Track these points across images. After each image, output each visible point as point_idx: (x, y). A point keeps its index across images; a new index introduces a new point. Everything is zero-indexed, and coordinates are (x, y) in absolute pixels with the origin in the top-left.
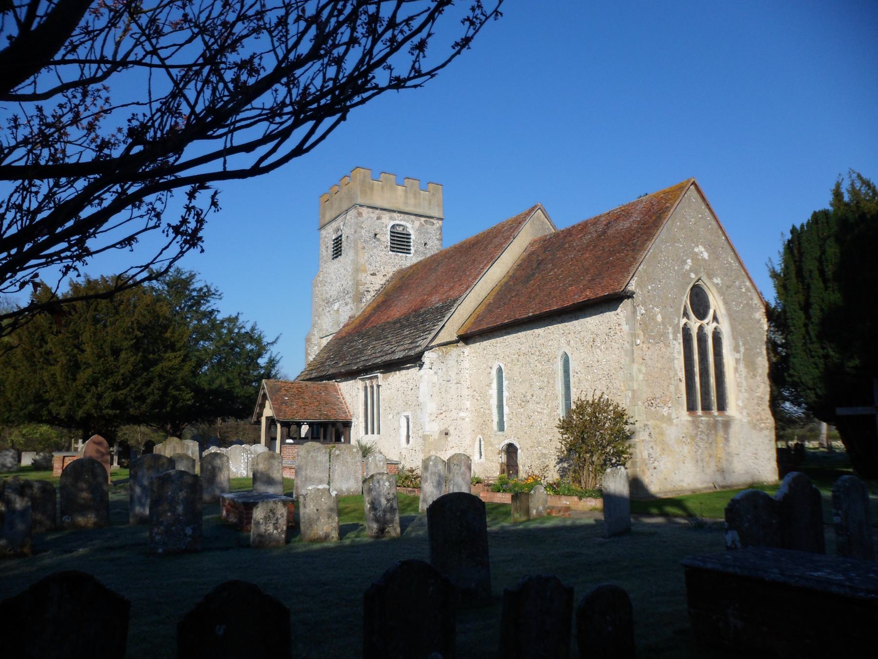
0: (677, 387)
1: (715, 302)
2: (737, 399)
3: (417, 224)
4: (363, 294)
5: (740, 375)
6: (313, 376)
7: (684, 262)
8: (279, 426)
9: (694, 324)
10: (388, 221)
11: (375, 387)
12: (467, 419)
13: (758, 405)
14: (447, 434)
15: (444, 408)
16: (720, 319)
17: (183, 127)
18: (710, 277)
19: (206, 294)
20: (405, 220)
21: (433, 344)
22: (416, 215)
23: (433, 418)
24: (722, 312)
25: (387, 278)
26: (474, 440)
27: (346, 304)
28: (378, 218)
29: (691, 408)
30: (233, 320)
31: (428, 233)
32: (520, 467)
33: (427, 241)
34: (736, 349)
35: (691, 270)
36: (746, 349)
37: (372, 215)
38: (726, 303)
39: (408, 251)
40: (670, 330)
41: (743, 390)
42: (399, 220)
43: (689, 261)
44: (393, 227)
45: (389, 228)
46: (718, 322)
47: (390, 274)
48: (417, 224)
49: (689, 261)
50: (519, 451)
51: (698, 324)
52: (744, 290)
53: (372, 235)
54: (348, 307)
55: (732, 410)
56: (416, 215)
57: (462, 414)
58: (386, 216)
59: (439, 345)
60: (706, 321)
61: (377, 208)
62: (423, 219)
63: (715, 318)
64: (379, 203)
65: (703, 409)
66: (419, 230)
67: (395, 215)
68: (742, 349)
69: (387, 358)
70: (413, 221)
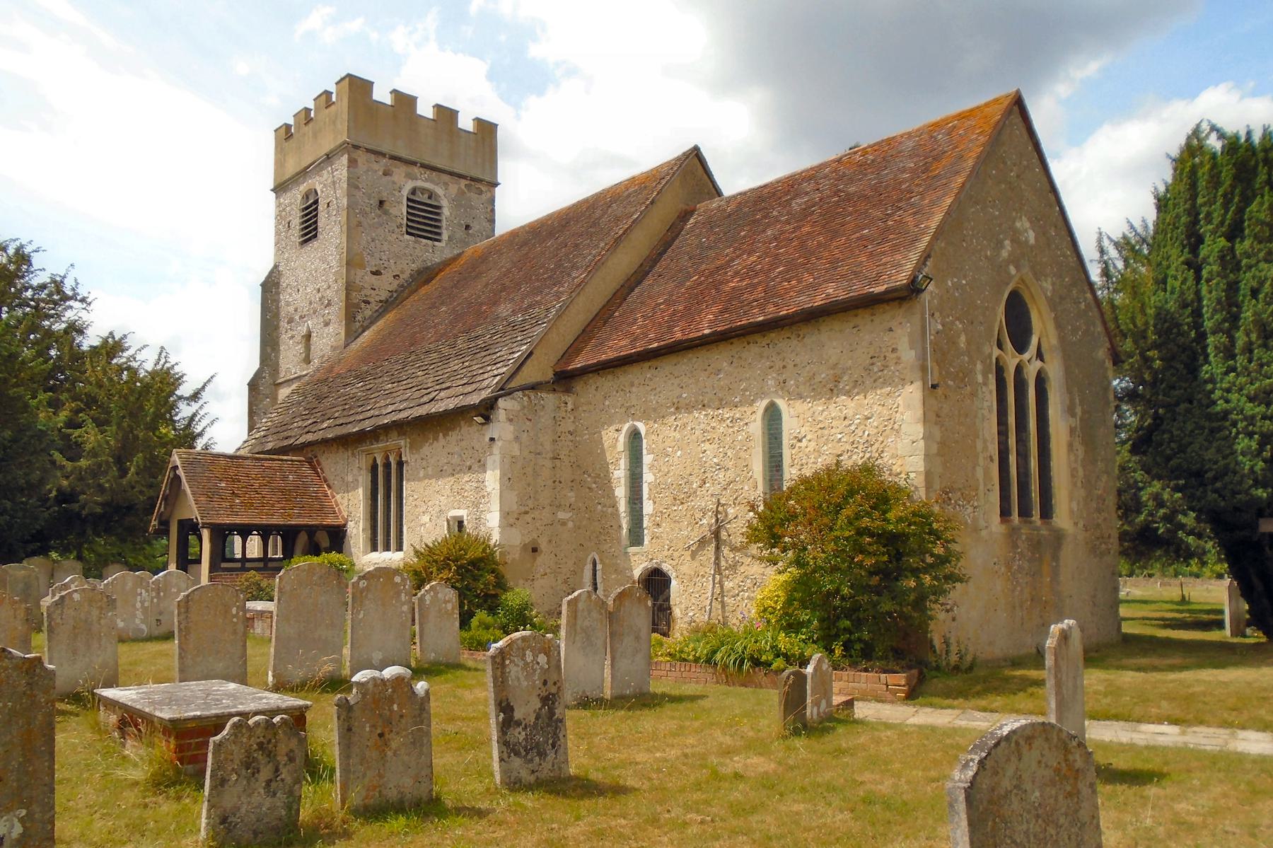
0: (987, 472)
1: (1042, 326)
2: (1071, 499)
3: (453, 189)
4: (357, 306)
5: (1077, 456)
6: (269, 446)
7: (1000, 245)
8: (206, 534)
9: (1012, 361)
10: (405, 183)
11: (394, 466)
12: (570, 524)
13: (1099, 511)
14: (535, 550)
15: (530, 503)
16: (1046, 357)
17: (85, 348)
18: (1038, 276)
19: (58, 294)
20: (432, 182)
21: (512, 385)
22: (451, 174)
23: (512, 521)
24: (1052, 339)
25: (401, 281)
26: (579, 563)
27: (327, 324)
28: (386, 173)
29: (1005, 513)
30: (112, 347)
31: (472, 207)
32: (677, 612)
33: (469, 222)
34: (1070, 411)
35: (1008, 262)
36: (1084, 412)
37: (376, 166)
38: (1059, 326)
39: (435, 236)
40: (979, 367)
41: (1079, 484)
42: (423, 181)
43: (1007, 242)
44: (414, 191)
45: (405, 192)
46: (1042, 360)
47: (406, 276)
48: (453, 189)
49: (1007, 242)
50: (674, 583)
51: (1016, 361)
52: (1083, 306)
53: (375, 202)
54: (331, 328)
55: (1063, 517)
56: (451, 174)
57: (562, 515)
58: (399, 172)
59: (523, 389)
60: (1026, 356)
61: (384, 155)
62: (463, 182)
63: (1040, 355)
64: (386, 147)
65: (1042, 517)
66: (457, 202)
67: (416, 170)
68: (1078, 410)
69: (422, 411)
70: (446, 184)
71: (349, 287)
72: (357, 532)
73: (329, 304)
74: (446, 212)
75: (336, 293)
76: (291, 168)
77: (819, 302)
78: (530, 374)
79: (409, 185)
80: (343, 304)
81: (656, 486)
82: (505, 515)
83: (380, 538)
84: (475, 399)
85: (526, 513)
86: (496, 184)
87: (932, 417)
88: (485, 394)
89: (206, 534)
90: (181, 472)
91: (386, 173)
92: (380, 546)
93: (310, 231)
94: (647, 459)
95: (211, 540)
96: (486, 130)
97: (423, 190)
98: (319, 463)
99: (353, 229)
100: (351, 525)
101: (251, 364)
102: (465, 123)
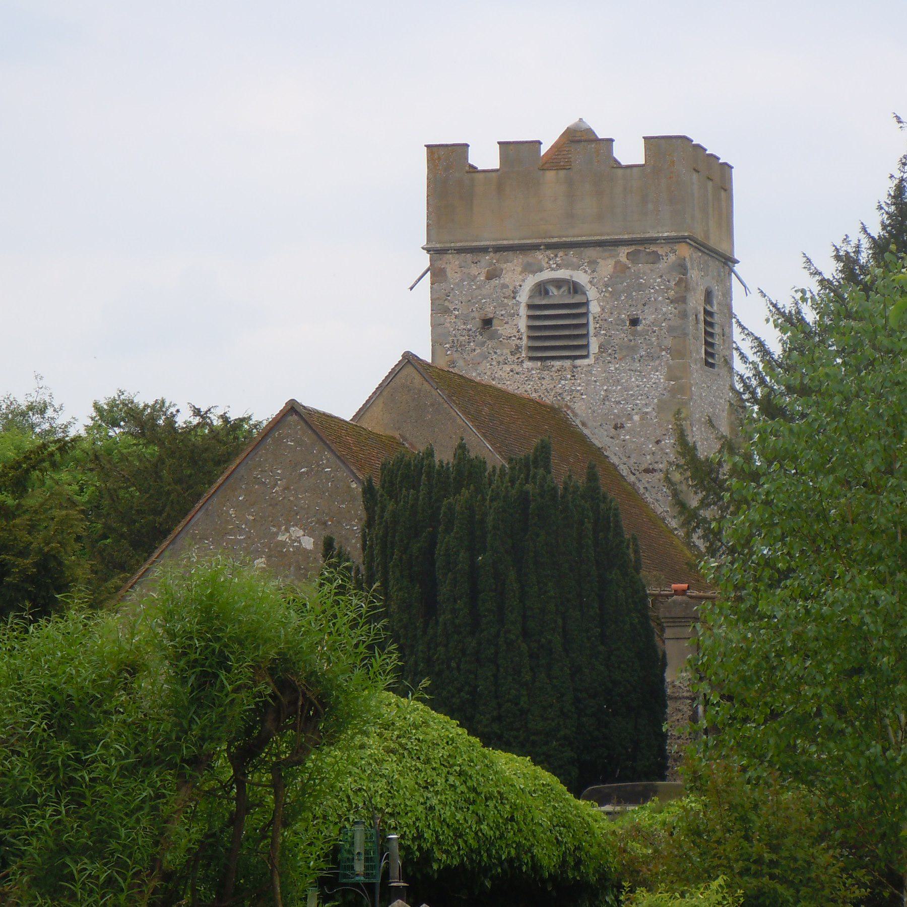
3: (606, 267)
28: (490, 276)
37: (474, 270)
44: (541, 289)
45: (523, 297)
48: (606, 267)
74: (594, 308)
79: (531, 281)
97: (558, 283)
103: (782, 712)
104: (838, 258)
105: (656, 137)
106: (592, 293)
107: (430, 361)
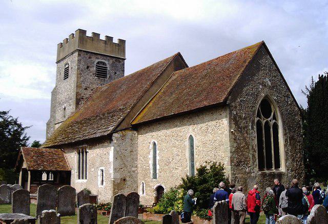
0: (253, 156)
1: (276, 110)
3: (111, 61)
8: (29, 172)
14: (124, 180)
27: (70, 105)
28: (90, 58)
37: (86, 56)
44: (98, 63)
45: (95, 63)
48: (111, 61)
60: (269, 119)
66: (112, 65)
71: (77, 94)
72: (75, 173)
73: (71, 99)
74: (108, 69)
75: (73, 95)
76: (61, 57)
77: (98, 135)
78: (124, 125)
79: (97, 61)
80: (75, 99)
81: (159, 160)
82: (115, 169)
83: (81, 175)
84: (106, 134)
85: (122, 168)
86: (125, 59)
87: (234, 138)
88: (109, 132)
89: (29, 172)
90: (23, 154)
91: (90, 58)
92: (81, 178)
93: (66, 76)
94: (158, 152)
95: (31, 175)
96: (122, 42)
97: (101, 62)
98: (86, 152)
99: (79, 75)
100: (72, 171)
101: (48, 117)
102: (115, 41)
103: (208, 182)
104: (319, 78)
105: (185, 63)
106: (108, 66)
107: (3, 120)
